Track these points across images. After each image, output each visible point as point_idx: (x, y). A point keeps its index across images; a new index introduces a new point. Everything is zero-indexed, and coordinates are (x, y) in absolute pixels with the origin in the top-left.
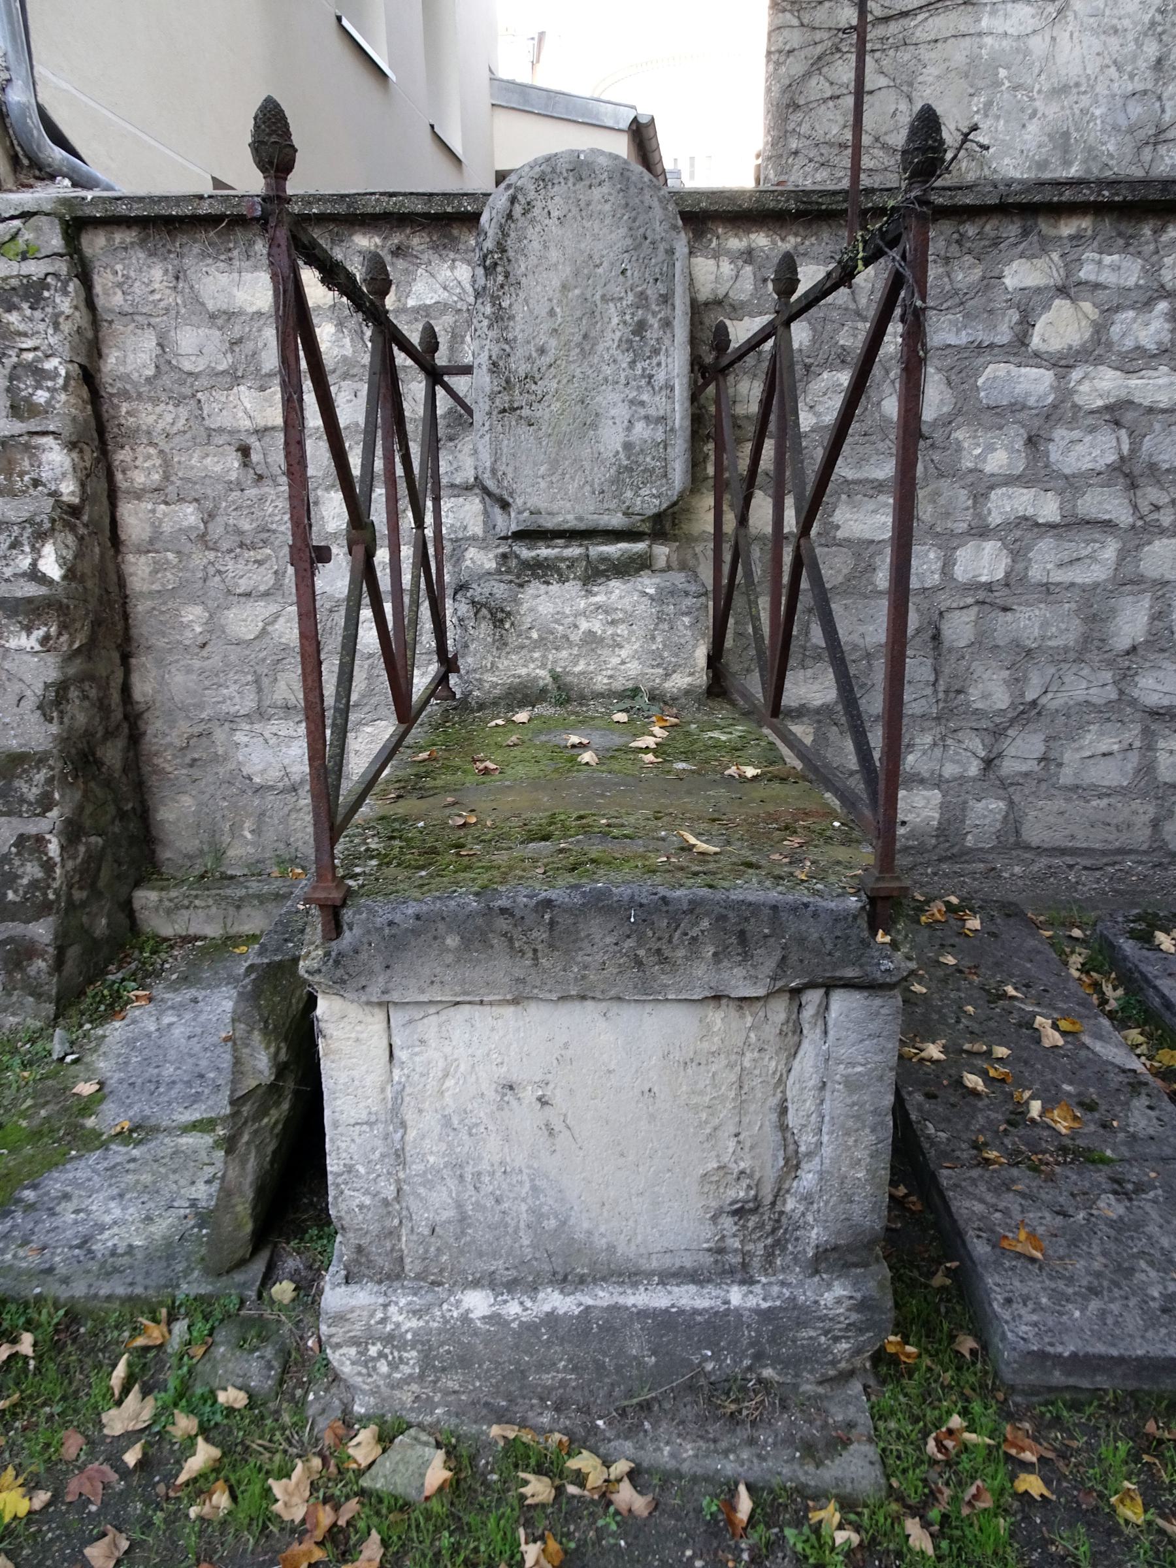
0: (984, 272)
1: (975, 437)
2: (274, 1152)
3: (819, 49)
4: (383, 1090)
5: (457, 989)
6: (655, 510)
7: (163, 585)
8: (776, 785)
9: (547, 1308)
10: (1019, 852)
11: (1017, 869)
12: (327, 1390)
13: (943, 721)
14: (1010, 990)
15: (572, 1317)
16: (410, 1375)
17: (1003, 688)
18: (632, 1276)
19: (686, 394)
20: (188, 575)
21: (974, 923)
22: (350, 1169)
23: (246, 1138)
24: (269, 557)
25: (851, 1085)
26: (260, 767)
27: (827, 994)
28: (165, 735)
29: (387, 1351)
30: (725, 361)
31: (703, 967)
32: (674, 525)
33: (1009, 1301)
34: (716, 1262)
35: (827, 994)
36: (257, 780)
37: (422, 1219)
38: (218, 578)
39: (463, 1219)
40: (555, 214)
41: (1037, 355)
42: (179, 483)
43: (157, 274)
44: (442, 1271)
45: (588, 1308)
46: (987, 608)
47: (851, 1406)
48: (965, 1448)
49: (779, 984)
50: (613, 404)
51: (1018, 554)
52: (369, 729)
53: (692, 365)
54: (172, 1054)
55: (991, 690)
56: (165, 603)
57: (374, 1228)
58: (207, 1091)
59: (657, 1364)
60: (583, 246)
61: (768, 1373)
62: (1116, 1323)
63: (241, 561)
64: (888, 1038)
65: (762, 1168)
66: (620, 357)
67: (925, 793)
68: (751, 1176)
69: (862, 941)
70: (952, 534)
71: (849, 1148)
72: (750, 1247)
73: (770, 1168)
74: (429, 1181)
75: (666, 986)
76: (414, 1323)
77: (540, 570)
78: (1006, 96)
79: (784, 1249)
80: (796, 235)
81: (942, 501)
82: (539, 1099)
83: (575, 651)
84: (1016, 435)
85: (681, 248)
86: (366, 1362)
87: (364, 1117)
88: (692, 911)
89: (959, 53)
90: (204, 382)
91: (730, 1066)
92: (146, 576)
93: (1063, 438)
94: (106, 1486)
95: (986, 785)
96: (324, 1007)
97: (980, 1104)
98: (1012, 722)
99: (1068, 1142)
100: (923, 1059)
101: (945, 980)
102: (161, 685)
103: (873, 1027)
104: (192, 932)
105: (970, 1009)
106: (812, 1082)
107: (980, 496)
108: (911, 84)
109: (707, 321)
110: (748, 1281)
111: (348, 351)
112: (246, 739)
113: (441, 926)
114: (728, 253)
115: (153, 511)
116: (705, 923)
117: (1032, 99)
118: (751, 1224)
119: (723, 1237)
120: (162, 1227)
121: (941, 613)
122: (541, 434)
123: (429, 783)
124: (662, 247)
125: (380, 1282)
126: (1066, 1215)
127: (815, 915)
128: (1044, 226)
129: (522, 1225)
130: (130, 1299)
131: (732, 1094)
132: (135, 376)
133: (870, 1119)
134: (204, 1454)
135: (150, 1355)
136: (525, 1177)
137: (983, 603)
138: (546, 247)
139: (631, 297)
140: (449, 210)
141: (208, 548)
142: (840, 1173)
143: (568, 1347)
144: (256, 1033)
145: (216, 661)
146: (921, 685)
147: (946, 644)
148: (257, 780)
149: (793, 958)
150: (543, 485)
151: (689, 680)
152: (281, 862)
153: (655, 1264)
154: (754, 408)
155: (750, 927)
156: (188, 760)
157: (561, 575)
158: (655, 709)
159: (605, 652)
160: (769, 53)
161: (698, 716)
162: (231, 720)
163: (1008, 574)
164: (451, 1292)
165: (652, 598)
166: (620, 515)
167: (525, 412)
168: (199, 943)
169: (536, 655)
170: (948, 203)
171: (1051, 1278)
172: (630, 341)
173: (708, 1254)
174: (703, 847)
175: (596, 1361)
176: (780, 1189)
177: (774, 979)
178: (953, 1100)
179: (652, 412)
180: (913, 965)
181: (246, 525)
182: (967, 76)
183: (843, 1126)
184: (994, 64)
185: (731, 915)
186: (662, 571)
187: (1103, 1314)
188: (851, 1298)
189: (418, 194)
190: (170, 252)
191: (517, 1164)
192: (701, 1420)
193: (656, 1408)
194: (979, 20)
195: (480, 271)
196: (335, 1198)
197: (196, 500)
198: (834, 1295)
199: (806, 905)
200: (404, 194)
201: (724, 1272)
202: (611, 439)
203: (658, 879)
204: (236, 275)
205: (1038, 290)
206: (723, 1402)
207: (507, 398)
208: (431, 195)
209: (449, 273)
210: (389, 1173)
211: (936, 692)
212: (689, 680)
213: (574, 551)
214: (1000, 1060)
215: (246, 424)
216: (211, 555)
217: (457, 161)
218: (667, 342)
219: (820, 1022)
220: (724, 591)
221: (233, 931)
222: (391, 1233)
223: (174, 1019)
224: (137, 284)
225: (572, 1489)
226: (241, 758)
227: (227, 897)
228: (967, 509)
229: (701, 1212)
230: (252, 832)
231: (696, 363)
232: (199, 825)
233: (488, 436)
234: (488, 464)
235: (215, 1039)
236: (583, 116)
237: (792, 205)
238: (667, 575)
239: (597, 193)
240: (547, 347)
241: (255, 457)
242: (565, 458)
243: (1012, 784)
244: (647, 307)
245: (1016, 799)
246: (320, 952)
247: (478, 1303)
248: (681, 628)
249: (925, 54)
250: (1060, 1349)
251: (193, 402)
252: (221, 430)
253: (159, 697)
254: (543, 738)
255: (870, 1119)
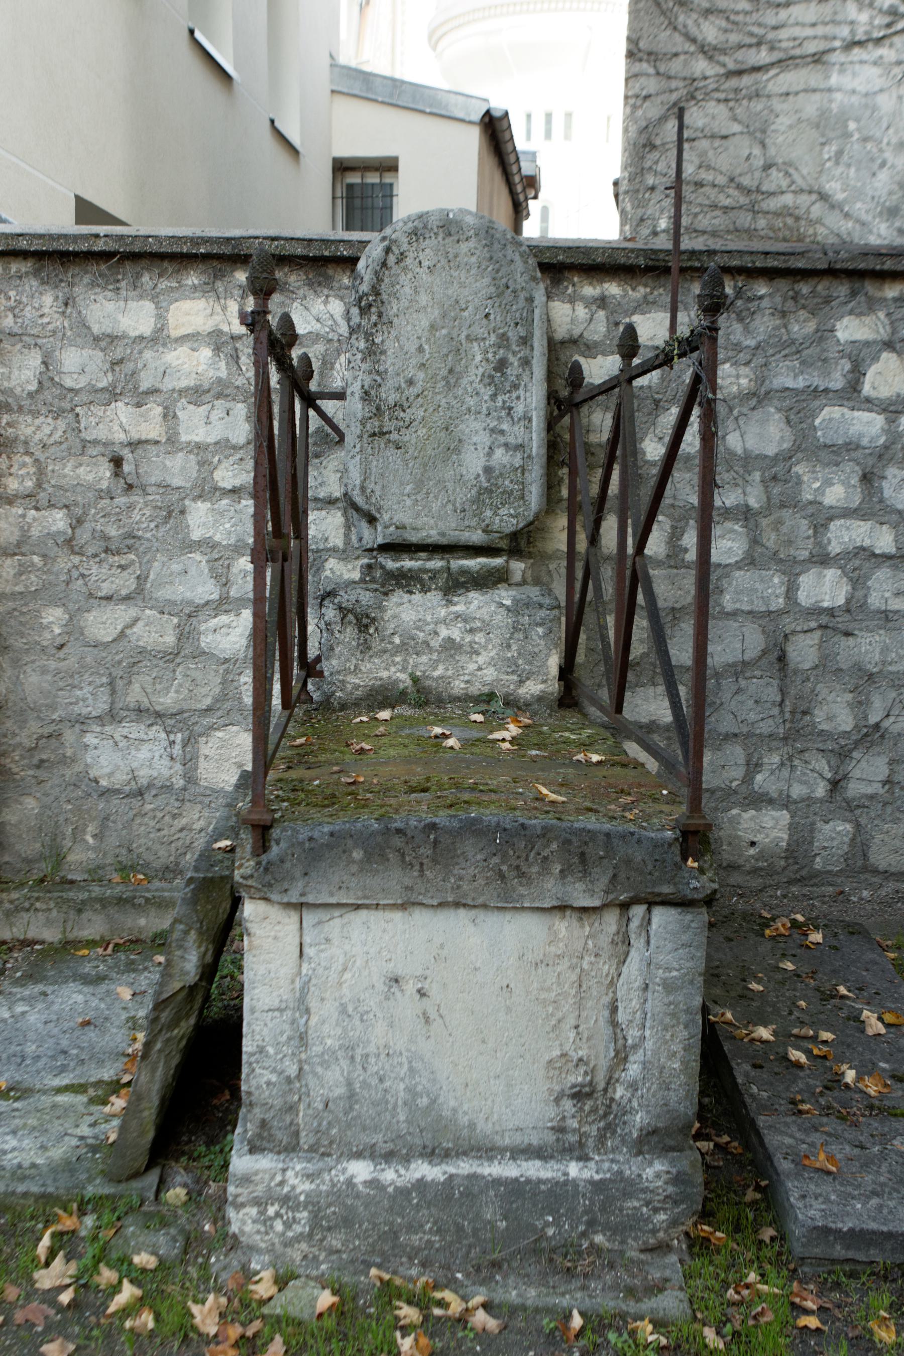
0: (818, 324)
1: (814, 472)
2: (177, 1066)
3: (674, 97)
4: (293, 982)
5: (360, 894)
6: (512, 529)
7: (26, 587)
8: (618, 770)
9: (418, 1175)
10: (867, 876)
11: (865, 894)
12: (226, 1255)
13: (790, 742)
14: (842, 990)
15: (438, 1183)
16: (301, 1234)
17: (847, 711)
18: (488, 1151)
19: (543, 425)
20: (52, 577)
21: (816, 937)
22: (261, 1050)
23: (158, 1046)
24: (132, 563)
25: (669, 987)
26: (107, 770)
27: (649, 910)
28: (15, 735)
29: (283, 1211)
30: (578, 398)
31: (552, 881)
32: (529, 543)
33: (804, 1197)
34: (558, 1140)
35: (649, 910)
36: (104, 783)
37: (318, 1094)
38: (80, 582)
39: (352, 1096)
40: (426, 263)
41: (868, 400)
42: (50, 490)
43: (48, 300)
44: (331, 1143)
45: (451, 1177)
46: (829, 631)
47: (670, 1266)
48: (759, 1294)
49: (611, 897)
50: (476, 432)
51: (858, 582)
52: (220, 734)
53: (549, 399)
54: (31, 1035)
55: (836, 713)
56: (26, 604)
57: (278, 1103)
58: (72, 1064)
59: (507, 1228)
60: (450, 292)
61: (599, 1239)
62: (890, 1212)
63: (105, 565)
64: (697, 948)
65: (596, 1057)
66: (483, 391)
67: (773, 813)
68: (587, 1064)
69: (676, 864)
70: (795, 561)
71: (666, 1042)
72: (585, 1128)
73: (603, 1059)
74: (325, 1061)
75: (522, 896)
76: (307, 1186)
77: (405, 581)
78: (856, 147)
79: (614, 1132)
80: (646, 286)
81: (784, 529)
82: (419, 991)
83: (435, 656)
84: (851, 472)
85: (540, 295)
86: (265, 1221)
87: (276, 1004)
88: (544, 835)
89: (810, 106)
90: (84, 397)
91: (572, 968)
92: (10, 577)
93: (895, 476)
94: (46, 1317)
95: (832, 807)
96: (250, 909)
97: (801, 1074)
98: (857, 744)
99: (877, 1103)
100: (753, 1040)
101: (782, 983)
102: (15, 684)
103: (685, 938)
104: (31, 935)
105: (802, 1004)
106: (637, 984)
107: (820, 526)
108: (764, 131)
109: (563, 358)
110: (584, 1158)
111: (223, 373)
112: (96, 741)
113: (350, 842)
114: (583, 298)
115: (24, 516)
116: (554, 846)
117: (881, 150)
118: (587, 1108)
119: (564, 1118)
120: (57, 1153)
121: (786, 636)
122: (407, 456)
123: (311, 759)
124: (522, 295)
125: (279, 1153)
126: (862, 1147)
127: (639, 841)
128: (870, 287)
129: (400, 1102)
130: (43, 1196)
131: (573, 992)
132: (18, 390)
133: (683, 1017)
134: (128, 1292)
135: (65, 1238)
136: (404, 1060)
137: (826, 627)
138: (416, 292)
139: (493, 338)
140: (326, 253)
141: (74, 553)
142: (659, 1068)
143: (434, 1210)
144: (193, 932)
145: (72, 662)
146: (768, 705)
147: (792, 666)
148: (104, 783)
149: (622, 876)
150: (408, 502)
151: (542, 687)
152: (123, 869)
153: (507, 1141)
154: (605, 436)
155: (589, 850)
156: (35, 761)
157: (423, 586)
158: (509, 712)
159: (464, 658)
160: (626, 97)
161: (550, 721)
162: (82, 721)
163: (848, 601)
164: (338, 1161)
165: (508, 610)
166: (480, 532)
167: (394, 436)
168: (37, 947)
169: (398, 659)
170: (783, 266)
171: (841, 1184)
172: (491, 377)
173: (551, 1133)
174: (553, 797)
175: (456, 1224)
176: (611, 1078)
177: (607, 892)
178: (776, 1070)
179: (512, 440)
180: (715, 886)
181: (113, 531)
182: (817, 126)
183: (661, 1022)
184: (843, 118)
185: (574, 839)
186: (518, 585)
187: (880, 1207)
188: (668, 1172)
189: (298, 239)
190: (61, 281)
191: (398, 1048)
192: (544, 1275)
193: (505, 1266)
194: (827, 77)
195: (355, 311)
196: (248, 1075)
197: (66, 507)
198: (654, 1171)
199: (632, 834)
200: (286, 239)
201: (564, 1150)
202: (473, 463)
203: (518, 813)
204: (122, 303)
205: (867, 344)
206: (562, 1261)
207: (377, 424)
208: (310, 240)
209: (322, 307)
210: (293, 1054)
211: (782, 712)
212: (542, 687)
213: (436, 563)
214: (825, 1042)
215: (121, 437)
216: (76, 559)
217: (293, 151)
218: (526, 378)
219: (644, 934)
220: (576, 606)
221: (71, 936)
222: (291, 1108)
223: (27, 1008)
224: (28, 308)
225: (437, 1312)
226: (89, 761)
227: (69, 900)
228: (808, 538)
229: (546, 1094)
230: (95, 836)
231: (552, 397)
232: (40, 828)
233: (358, 458)
234: (358, 482)
235: (72, 1024)
236: (431, 106)
237: (642, 262)
238: (522, 589)
239: (464, 247)
240: (416, 379)
241: (126, 468)
242: (429, 479)
243: (858, 806)
244: (508, 348)
245: (863, 821)
246: (252, 863)
247: (360, 1171)
248: (535, 637)
249: (778, 105)
250: (840, 1225)
251: (71, 416)
252: (95, 442)
253: (12, 697)
254: (407, 731)
255: (683, 1017)
